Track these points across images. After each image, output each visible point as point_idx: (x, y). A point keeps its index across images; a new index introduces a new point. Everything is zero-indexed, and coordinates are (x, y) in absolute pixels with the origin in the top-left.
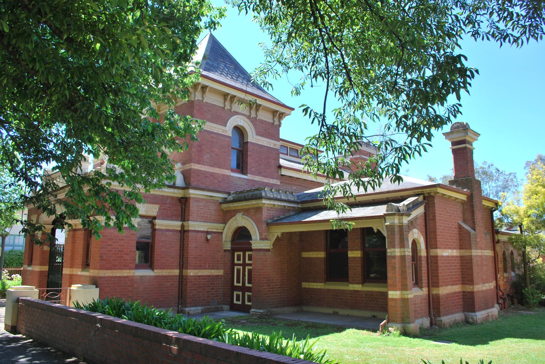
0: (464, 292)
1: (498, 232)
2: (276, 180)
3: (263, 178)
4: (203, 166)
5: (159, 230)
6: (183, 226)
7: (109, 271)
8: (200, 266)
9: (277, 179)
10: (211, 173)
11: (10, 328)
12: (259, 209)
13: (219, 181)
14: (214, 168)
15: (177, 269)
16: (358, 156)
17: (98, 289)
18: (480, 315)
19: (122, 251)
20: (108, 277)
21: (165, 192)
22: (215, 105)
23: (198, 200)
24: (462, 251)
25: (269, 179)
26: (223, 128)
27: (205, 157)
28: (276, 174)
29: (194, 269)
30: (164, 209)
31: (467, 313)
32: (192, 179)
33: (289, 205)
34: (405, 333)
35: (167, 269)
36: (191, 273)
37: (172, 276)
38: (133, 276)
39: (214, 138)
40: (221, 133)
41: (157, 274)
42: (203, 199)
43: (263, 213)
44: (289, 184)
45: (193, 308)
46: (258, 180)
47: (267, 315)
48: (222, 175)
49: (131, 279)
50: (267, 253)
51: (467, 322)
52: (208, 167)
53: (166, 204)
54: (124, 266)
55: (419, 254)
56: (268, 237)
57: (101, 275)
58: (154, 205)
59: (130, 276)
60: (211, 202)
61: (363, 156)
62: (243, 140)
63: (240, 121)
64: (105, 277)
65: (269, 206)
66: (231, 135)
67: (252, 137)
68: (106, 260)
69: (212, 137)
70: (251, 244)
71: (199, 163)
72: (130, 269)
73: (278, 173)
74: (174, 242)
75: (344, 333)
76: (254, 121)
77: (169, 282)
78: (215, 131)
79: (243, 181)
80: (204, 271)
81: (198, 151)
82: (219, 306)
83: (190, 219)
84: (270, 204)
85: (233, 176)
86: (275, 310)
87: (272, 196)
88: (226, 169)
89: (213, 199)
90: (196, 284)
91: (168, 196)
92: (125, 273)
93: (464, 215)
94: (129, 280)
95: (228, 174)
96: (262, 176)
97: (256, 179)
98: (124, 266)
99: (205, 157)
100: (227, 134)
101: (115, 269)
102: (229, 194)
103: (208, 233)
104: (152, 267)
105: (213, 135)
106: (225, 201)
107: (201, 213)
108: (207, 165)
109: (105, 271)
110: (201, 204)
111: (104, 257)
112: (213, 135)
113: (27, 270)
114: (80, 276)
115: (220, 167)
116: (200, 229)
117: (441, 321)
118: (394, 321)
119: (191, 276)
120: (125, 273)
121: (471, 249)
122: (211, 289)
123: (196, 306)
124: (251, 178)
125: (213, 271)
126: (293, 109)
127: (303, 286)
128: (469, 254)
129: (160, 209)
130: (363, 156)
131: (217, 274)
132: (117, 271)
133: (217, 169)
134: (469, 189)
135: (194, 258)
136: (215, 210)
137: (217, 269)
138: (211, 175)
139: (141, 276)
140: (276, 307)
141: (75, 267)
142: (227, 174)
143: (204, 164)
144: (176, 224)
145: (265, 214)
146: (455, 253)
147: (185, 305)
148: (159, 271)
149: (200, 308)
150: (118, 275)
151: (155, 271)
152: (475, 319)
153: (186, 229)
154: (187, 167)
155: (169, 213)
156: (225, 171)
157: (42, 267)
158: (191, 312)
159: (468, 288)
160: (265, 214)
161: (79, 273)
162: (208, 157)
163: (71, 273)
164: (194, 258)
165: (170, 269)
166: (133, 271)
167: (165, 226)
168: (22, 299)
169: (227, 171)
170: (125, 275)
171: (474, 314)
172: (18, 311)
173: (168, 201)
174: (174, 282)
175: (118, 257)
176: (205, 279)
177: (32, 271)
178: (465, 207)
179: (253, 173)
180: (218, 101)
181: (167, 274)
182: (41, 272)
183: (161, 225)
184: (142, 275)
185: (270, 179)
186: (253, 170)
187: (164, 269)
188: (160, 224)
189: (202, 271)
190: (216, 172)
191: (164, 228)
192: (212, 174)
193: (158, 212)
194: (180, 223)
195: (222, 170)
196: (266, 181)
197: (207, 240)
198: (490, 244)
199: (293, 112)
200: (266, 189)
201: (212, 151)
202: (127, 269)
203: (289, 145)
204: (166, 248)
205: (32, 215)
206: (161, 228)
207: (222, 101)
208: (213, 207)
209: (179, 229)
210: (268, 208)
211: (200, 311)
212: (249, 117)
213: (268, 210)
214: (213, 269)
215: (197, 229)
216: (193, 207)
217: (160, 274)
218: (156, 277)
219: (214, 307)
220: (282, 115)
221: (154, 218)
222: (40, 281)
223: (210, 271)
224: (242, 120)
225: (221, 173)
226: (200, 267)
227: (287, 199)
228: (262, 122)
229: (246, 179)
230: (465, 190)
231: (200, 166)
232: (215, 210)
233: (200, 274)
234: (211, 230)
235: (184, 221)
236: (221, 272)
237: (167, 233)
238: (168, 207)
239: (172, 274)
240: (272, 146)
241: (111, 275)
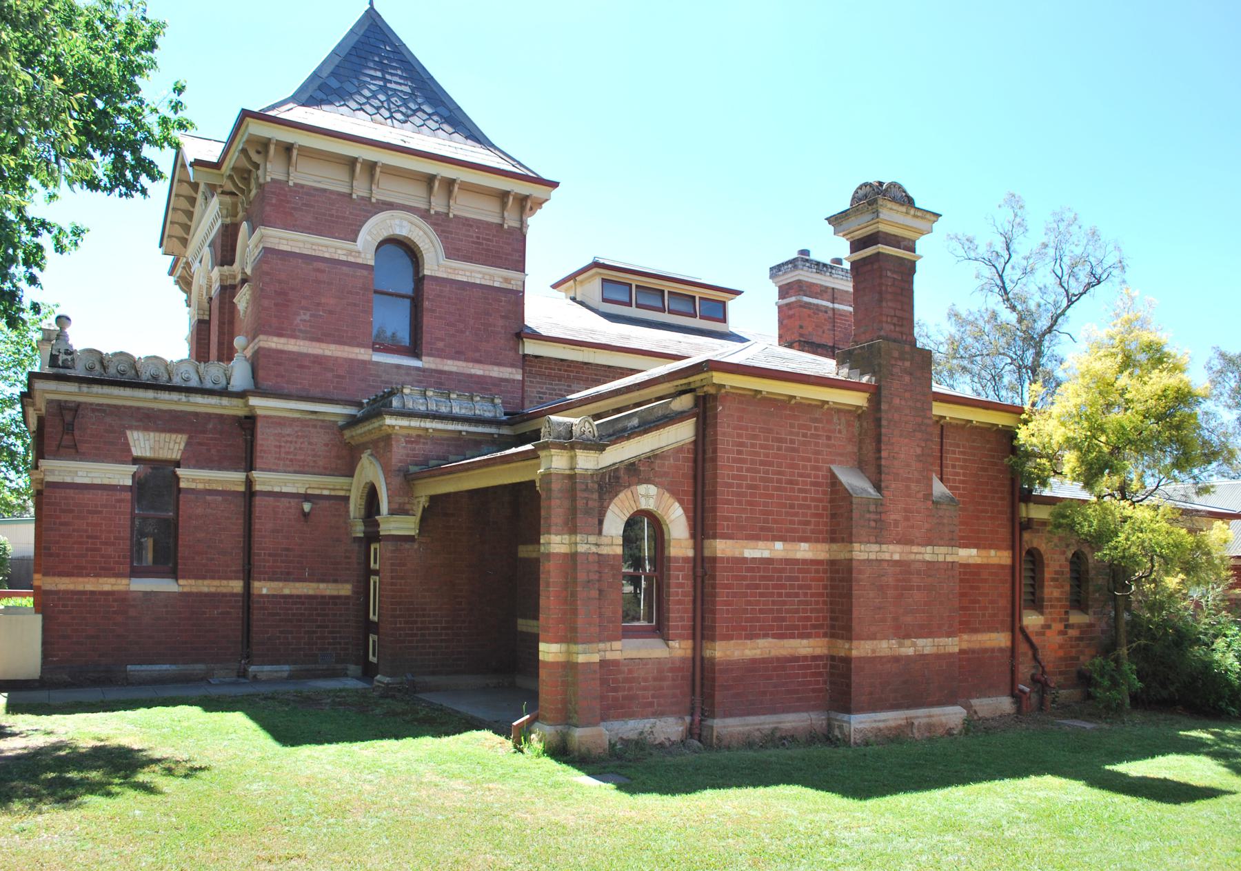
0: (833, 658)
1: (1028, 497)
2: (509, 370)
3: (471, 365)
4: (292, 341)
5: (188, 490)
6: (249, 483)
7: (66, 580)
8: (288, 573)
9: (512, 366)
10: (316, 356)
12: (387, 439)
13: (339, 376)
14: (324, 345)
15: (237, 578)
16: (793, 299)
18: (860, 723)
19: (96, 537)
20: (66, 592)
21: (196, 404)
22: (325, 190)
23: (280, 422)
24: (835, 546)
25: (486, 367)
26: (348, 245)
27: (298, 320)
28: (511, 354)
29: (271, 579)
30: (200, 444)
31: (833, 714)
33: (480, 429)
34: (560, 752)
35: (213, 578)
37: (224, 595)
38: (127, 592)
39: (323, 271)
40: (344, 258)
41: (186, 589)
42: (294, 420)
43: (395, 449)
44: (560, 378)
45: (267, 668)
46: (454, 369)
47: (399, 691)
48: (346, 359)
49: (123, 598)
50: (407, 546)
51: (828, 738)
52: (307, 343)
53: (204, 432)
54: (102, 568)
55: (666, 553)
56: (408, 507)
58: (174, 436)
59: (119, 592)
60: (315, 426)
61: (806, 299)
63: (401, 226)
64: (57, 592)
65: (414, 433)
66: (372, 263)
67: (436, 264)
68: (58, 555)
69: (318, 270)
70: (378, 525)
71: (280, 335)
72: (118, 575)
73: (517, 351)
75: (401, 742)
76: (441, 223)
78: (327, 255)
79: (408, 374)
80: (298, 585)
81: (276, 305)
82: (339, 666)
84: (409, 427)
85: (377, 363)
86: (428, 679)
87: (423, 408)
88: (359, 345)
89: (321, 417)
90: (278, 614)
92: (107, 584)
93: (860, 449)
94: (115, 600)
95: (366, 357)
96: (466, 360)
97: (446, 368)
98: (102, 568)
99: (299, 318)
100: (360, 261)
101: (80, 575)
102: (359, 405)
103: (307, 497)
104: (174, 574)
105: (321, 265)
106: (353, 422)
107: (288, 453)
109: (57, 579)
110: (288, 431)
112: (321, 265)
115: (340, 341)
116: (285, 490)
117: (712, 727)
118: (545, 719)
120: (107, 584)
121: (851, 542)
122: (319, 627)
123: (278, 662)
124: (433, 366)
125: (322, 586)
126: (554, 185)
127: (519, 628)
128: (847, 556)
129: (187, 444)
130: (806, 299)
131: (335, 593)
132: (86, 580)
133: (333, 347)
134: (874, 373)
135: (270, 555)
136: (326, 445)
137: (335, 581)
138: (314, 362)
139: (146, 593)
140: (433, 673)
142: (360, 357)
144: (233, 479)
145: (399, 452)
146: (863, 552)
147: (249, 658)
148: (192, 582)
149: (286, 667)
151: (181, 582)
152: (846, 730)
155: (213, 451)
156: (357, 350)
158: (260, 676)
159: (842, 647)
160: (399, 452)
162: (307, 317)
164: (270, 555)
165: (220, 578)
167: (204, 482)
169: (362, 350)
170: (107, 588)
171: (846, 717)
173: (210, 426)
175: (87, 549)
176: (303, 603)
178: (865, 424)
179: (441, 354)
180: (331, 180)
181: (213, 590)
183: (194, 480)
184: (148, 589)
185: (490, 367)
186: (440, 345)
187: (204, 578)
188: (189, 477)
189: (291, 584)
190: (328, 353)
191: (200, 486)
192: (318, 360)
194: (240, 476)
195: (346, 348)
196: (480, 372)
197: (306, 515)
198: (1004, 532)
199: (555, 193)
200: (406, 391)
201: (319, 304)
203: (635, 280)
206: (193, 486)
207: (346, 178)
208: (320, 439)
209: (242, 488)
210: (408, 436)
211: (285, 674)
212: (425, 215)
213: (407, 442)
214: (323, 581)
215: (277, 489)
216: (265, 438)
217: (194, 590)
219: (325, 667)
220: (526, 205)
223: (314, 585)
224: (405, 223)
225: (345, 355)
226: (287, 577)
227: (469, 413)
228: (468, 223)
229: (418, 369)
230: (865, 379)
231: (283, 340)
232: (326, 445)
233: (287, 592)
234: (317, 492)
236: (345, 590)
237: (208, 498)
238: (211, 439)
239: (224, 590)
240: (497, 284)
241: (71, 587)
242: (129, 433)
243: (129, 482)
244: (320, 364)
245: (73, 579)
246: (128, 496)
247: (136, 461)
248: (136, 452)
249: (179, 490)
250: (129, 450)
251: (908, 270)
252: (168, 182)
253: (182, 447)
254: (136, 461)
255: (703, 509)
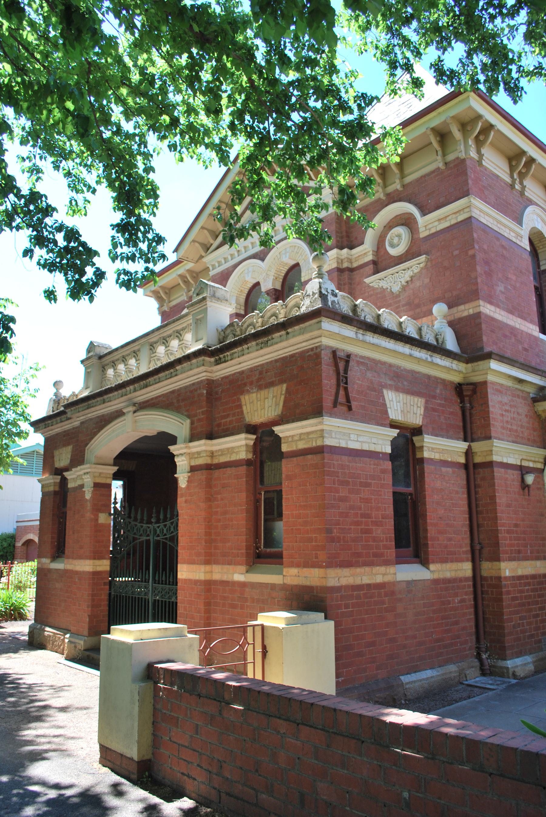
6: (468, 453)
7: (346, 572)
8: (519, 552)
11: (134, 768)
15: (467, 560)
17: (331, 624)
32: (485, 338)
36: (508, 569)
41: (436, 576)
42: (508, 388)
54: (375, 555)
57: (332, 582)
59: (389, 583)
62: (539, 266)
74: (457, 493)
77: (456, 595)
83: (493, 434)
91: (436, 378)
94: (386, 595)
108: (504, 309)
109: (339, 572)
111: (335, 533)
113: (50, 570)
114: (243, 585)
119: (506, 578)
133: (519, 320)
139: (408, 583)
141: (217, 563)
143: (498, 306)
149: (528, 659)
150: (366, 580)
153: (478, 459)
154: (465, 310)
157: (97, 562)
161: (239, 577)
163: (208, 577)
166: (391, 569)
167: (443, 451)
168: (166, 670)
170: (379, 579)
172: (155, 710)
174: (466, 594)
176: (529, 584)
177: (66, 571)
182: (95, 574)
184: (409, 579)
193: (425, 416)
194: (463, 446)
197: (524, 486)
202: (380, 565)
204: (445, 505)
205: (56, 448)
211: (531, 667)
218: (436, 582)
221: (418, 431)
222: (93, 595)
235: (473, 441)
237: (444, 469)
238: (440, 405)
242: (385, 391)
243: (388, 450)
244: (515, 336)
245: (353, 570)
246: (388, 465)
247: (393, 425)
248: (394, 414)
249: (422, 461)
250: (386, 412)
251: (66, 513)
252: (419, 106)
253: (422, 412)
254: (393, 425)
255: (476, 499)
